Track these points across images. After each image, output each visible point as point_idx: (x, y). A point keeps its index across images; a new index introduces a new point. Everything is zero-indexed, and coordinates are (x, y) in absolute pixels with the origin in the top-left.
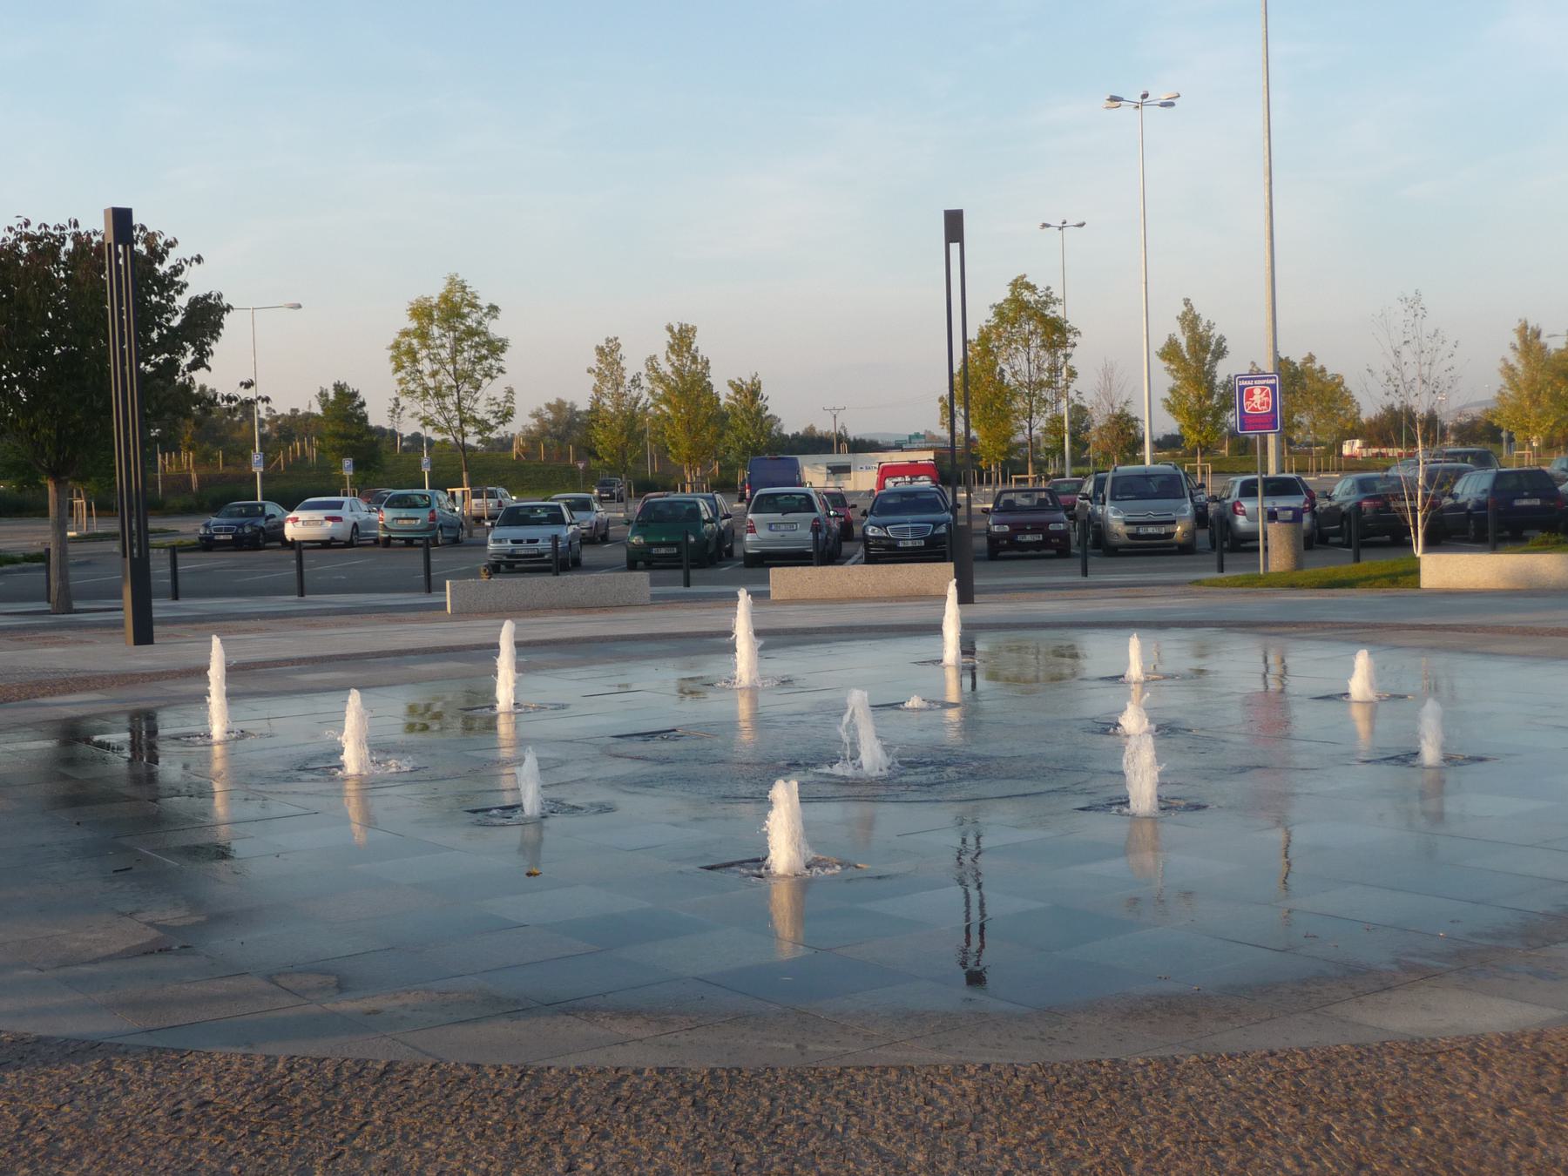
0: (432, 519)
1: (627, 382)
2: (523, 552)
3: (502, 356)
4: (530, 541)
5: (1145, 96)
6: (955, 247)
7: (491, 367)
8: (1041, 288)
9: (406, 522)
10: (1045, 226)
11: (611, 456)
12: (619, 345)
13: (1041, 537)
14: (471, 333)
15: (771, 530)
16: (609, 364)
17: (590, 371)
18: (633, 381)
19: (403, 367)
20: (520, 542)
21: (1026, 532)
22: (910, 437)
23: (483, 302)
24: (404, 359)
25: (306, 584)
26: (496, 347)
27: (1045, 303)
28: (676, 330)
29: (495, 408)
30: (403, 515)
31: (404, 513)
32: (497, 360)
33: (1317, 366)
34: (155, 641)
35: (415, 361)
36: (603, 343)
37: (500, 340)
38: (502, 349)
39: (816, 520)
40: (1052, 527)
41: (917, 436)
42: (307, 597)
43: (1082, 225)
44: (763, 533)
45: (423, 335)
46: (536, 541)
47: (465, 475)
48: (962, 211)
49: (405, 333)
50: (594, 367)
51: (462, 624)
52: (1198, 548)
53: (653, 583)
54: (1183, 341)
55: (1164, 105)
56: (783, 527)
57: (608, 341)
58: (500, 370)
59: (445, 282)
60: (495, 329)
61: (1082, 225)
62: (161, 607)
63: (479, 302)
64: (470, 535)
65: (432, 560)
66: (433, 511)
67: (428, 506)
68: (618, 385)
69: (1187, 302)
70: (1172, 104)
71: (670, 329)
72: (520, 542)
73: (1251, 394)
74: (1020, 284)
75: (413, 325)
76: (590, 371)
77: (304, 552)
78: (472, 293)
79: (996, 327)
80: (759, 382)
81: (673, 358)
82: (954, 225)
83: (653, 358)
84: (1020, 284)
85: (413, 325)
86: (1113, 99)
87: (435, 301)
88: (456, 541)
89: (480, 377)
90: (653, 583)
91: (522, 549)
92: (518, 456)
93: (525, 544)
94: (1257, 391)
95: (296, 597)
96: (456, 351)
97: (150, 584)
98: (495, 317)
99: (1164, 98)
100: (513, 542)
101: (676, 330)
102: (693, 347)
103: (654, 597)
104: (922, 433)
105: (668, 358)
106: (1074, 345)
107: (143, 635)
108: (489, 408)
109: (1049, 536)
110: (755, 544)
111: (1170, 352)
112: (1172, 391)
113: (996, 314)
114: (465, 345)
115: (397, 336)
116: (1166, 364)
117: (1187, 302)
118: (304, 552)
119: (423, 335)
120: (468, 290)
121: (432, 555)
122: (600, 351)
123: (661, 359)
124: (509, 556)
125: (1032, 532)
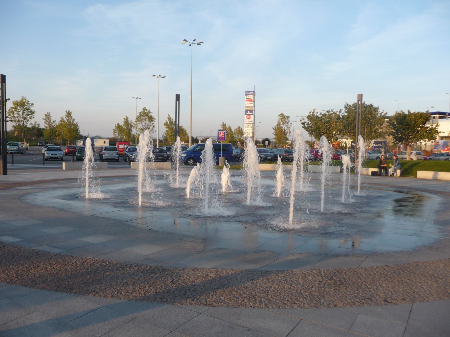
0: (19, 148)
1: (52, 122)
2: (54, 157)
3: (34, 114)
4: (55, 154)
5: (160, 76)
6: (178, 101)
7: (31, 117)
8: (148, 110)
9: (12, 149)
10: (133, 98)
11: (47, 137)
12: (50, 114)
13: (162, 158)
14: (27, 109)
15: (108, 154)
16: (48, 118)
17: (43, 119)
18: (53, 121)
19: (11, 115)
20: (53, 154)
21: (159, 157)
22: (95, 136)
23: (30, 102)
24: (11, 113)
25: (14, 162)
26: (32, 113)
27: (149, 113)
28: (67, 112)
29: (32, 125)
30: (12, 147)
31: (12, 147)
32: (33, 115)
33: (183, 128)
34: (8, 174)
35: (13, 114)
36: (46, 114)
37: (33, 111)
38: (34, 113)
39: (117, 152)
40: (164, 156)
41: (97, 136)
42: (14, 165)
43: (141, 98)
44: (106, 155)
45: (16, 108)
46: (57, 154)
47: (24, 139)
48: (179, 95)
49: (12, 108)
50: (44, 118)
51: (97, 171)
52: (64, 159)
53: (108, 164)
54: (168, 122)
55: (163, 78)
56: (111, 154)
57: (48, 113)
58: (34, 117)
59: (21, 98)
60: (32, 108)
61: (141, 98)
62: (9, 166)
63: (29, 102)
64: (25, 152)
65: (43, 158)
66: (19, 147)
67: (18, 145)
68: (50, 122)
69: (169, 115)
70: (164, 78)
71: (66, 112)
72: (53, 154)
73: (220, 133)
74: (144, 109)
75: (14, 106)
76: (43, 119)
77: (14, 155)
78: (28, 101)
79: (140, 117)
80: (78, 124)
81: (67, 117)
82: (178, 97)
83: (62, 117)
84: (144, 109)
85: (14, 106)
86: (154, 75)
87: (19, 102)
88: (22, 153)
89: (28, 119)
90: (108, 164)
91: (54, 156)
92: (16, 135)
93: (54, 155)
94: (222, 133)
95: (11, 165)
96: (23, 113)
97: (7, 161)
98: (33, 106)
99: (163, 77)
100: (51, 154)
101: (67, 112)
102: (71, 116)
103: (109, 167)
104: (98, 136)
105: (65, 118)
106: (154, 121)
107: (5, 173)
108: (30, 125)
109: (164, 157)
110: (104, 157)
111: (166, 124)
112: (166, 131)
113: (140, 114)
114: (25, 111)
115: (10, 108)
116: (165, 126)
117: (169, 115)
118: (14, 155)
119: (16, 108)
120: (26, 100)
121: (14, 156)
122: (46, 115)
123: (64, 117)
124: (50, 157)
125: (160, 157)
